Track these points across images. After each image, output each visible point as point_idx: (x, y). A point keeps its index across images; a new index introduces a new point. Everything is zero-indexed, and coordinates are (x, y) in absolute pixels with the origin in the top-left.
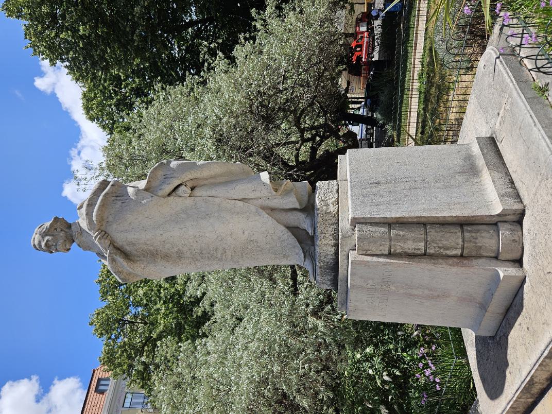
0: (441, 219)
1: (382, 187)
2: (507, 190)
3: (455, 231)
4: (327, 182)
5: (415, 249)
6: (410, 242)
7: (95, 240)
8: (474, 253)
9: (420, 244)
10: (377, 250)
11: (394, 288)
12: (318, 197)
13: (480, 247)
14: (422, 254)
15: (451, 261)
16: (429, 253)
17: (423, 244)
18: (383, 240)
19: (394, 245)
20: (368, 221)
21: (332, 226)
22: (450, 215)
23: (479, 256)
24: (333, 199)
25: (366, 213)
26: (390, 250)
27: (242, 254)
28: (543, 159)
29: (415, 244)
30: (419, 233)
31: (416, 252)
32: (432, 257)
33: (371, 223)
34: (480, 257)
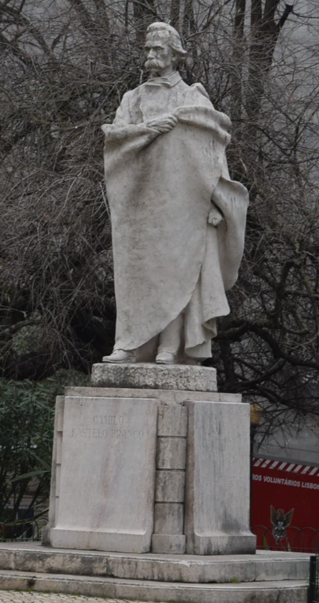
0: (191, 485)
1: (216, 435)
2: (213, 546)
3: (180, 497)
4: (216, 380)
5: (164, 460)
6: (170, 455)
8: (158, 513)
11: (116, 443)
13: (164, 518)
15: (152, 492)
16: (159, 474)
17: (169, 467)
20: (190, 418)
21: (175, 383)
24: (201, 386)
25: (198, 415)
26: (163, 437)
27: (136, 278)
30: (180, 465)
32: (156, 476)
33: (188, 421)
34: (155, 519)
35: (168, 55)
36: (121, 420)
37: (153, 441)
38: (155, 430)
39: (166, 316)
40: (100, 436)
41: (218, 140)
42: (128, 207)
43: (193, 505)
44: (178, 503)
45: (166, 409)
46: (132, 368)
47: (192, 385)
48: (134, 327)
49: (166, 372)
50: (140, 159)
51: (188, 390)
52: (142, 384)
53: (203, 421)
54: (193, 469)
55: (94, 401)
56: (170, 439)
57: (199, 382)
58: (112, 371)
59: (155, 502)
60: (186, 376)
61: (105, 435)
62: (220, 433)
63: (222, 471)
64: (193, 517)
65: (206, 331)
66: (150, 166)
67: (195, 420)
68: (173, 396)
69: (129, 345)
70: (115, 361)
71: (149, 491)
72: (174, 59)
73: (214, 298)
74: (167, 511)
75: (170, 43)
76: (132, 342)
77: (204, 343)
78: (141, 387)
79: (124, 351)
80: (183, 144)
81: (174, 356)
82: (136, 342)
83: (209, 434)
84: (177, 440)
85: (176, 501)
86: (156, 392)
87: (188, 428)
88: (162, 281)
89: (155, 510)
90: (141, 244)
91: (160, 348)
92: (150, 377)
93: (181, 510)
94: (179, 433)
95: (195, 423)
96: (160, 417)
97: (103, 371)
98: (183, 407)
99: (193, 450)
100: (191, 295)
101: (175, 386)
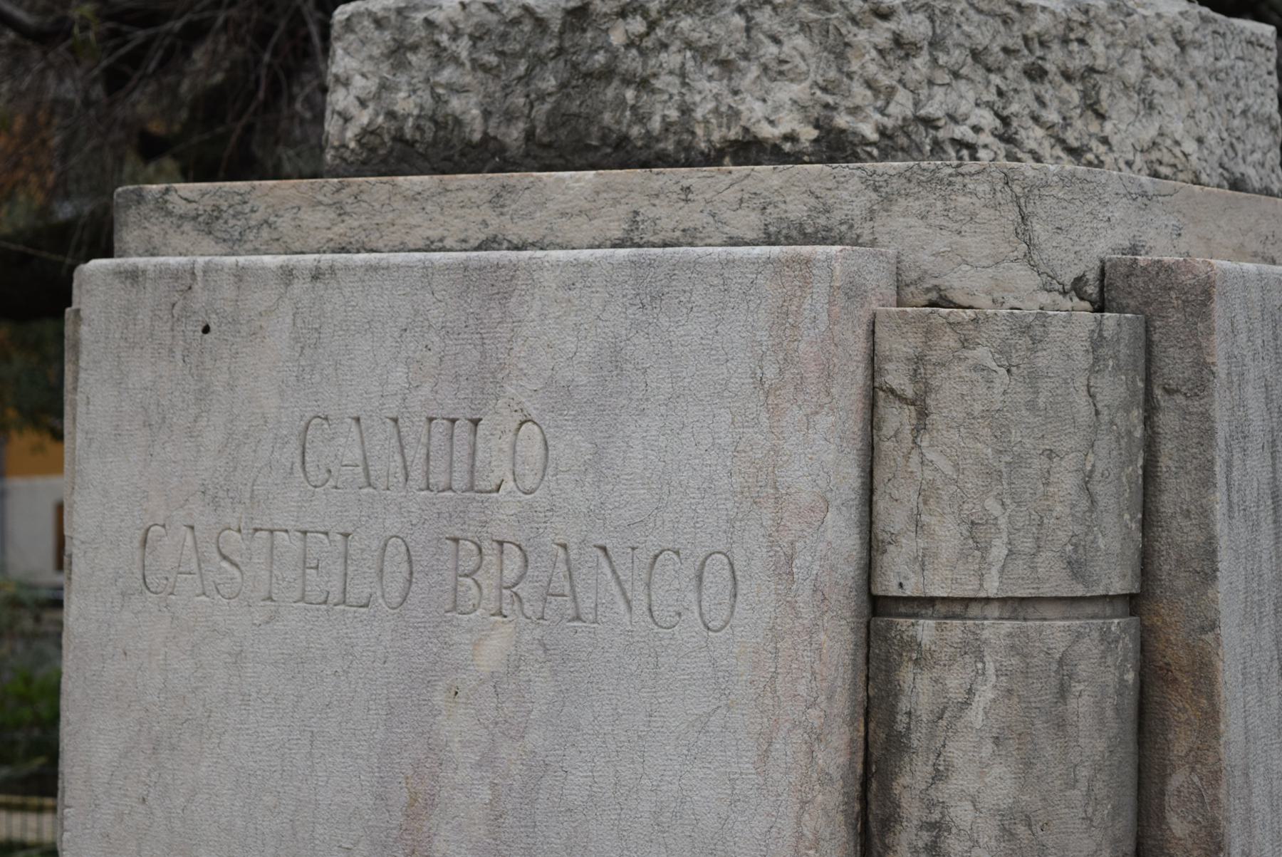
5: (937, 828)
10: (926, 494)
18: (1027, 545)
20: (1168, 421)
21: (986, 119)
24: (1190, 146)
26: (923, 604)
28: (924, 699)
33: (1150, 446)
38: (849, 542)
40: (358, 591)
45: (949, 340)
55: (298, 287)
56: (996, 630)
58: (462, 48)
60: (1077, 63)
61: (395, 589)
67: (1222, 430)
68: (1014, 215)
87: (1148, 518)
92: (778, 71)
94: (1076, 568)
95: (1219, 468)
96: (896, 418)
97: (398, 53)
98: (1110, 318)
99: (1211, 717)
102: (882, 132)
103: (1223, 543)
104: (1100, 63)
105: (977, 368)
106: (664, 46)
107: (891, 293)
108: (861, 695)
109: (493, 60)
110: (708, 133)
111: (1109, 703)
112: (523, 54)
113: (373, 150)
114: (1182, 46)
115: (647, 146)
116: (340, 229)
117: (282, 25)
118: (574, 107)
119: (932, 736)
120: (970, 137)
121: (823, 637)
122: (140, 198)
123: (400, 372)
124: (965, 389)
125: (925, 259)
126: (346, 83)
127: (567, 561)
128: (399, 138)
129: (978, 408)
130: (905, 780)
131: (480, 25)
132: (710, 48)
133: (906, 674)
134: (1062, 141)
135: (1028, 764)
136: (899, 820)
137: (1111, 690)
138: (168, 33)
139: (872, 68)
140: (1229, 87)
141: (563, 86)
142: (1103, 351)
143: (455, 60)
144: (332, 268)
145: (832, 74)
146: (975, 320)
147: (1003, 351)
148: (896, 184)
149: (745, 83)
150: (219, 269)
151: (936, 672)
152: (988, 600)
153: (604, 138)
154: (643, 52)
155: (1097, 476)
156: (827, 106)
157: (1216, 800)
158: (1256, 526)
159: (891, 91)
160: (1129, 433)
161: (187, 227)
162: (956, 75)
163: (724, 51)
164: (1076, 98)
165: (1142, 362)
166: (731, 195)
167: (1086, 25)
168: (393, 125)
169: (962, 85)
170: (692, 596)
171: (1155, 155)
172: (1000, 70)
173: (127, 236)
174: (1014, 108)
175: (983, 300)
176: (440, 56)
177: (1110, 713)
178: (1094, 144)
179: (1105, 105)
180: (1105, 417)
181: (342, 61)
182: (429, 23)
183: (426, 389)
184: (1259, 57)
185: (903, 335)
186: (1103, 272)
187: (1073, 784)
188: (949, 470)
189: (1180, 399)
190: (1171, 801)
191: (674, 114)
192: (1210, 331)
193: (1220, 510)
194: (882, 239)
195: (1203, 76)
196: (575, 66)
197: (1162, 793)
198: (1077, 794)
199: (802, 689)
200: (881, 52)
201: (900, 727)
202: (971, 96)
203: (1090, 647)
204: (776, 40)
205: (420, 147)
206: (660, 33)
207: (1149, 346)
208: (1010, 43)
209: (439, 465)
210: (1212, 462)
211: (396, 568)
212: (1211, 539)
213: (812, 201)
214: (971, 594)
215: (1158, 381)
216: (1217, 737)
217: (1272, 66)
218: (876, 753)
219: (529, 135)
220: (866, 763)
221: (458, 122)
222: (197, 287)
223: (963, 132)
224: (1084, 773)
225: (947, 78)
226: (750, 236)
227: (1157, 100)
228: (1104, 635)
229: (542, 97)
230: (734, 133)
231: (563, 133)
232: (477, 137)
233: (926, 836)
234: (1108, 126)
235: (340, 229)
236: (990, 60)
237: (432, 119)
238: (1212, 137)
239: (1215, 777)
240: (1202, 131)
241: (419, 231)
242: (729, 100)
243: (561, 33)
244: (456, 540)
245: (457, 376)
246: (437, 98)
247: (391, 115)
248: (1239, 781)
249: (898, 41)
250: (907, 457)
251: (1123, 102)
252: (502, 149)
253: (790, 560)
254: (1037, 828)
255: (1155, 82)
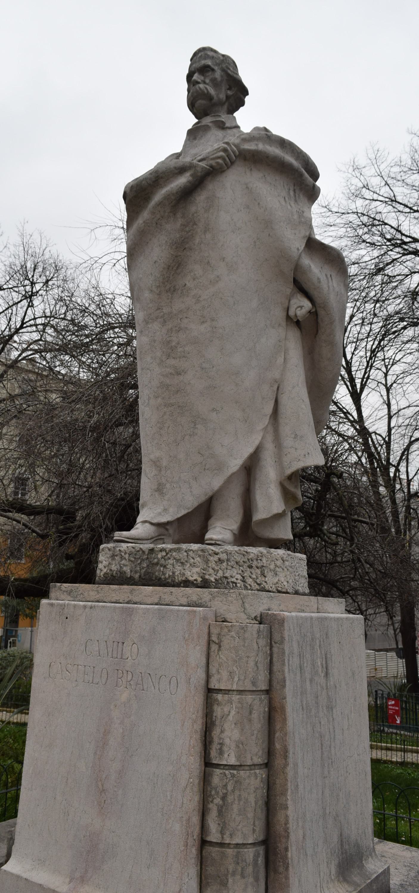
1: (322, 680)
3: (257, 829)
5: (222, 744)
7: (224, 143)
8: (210, 870)
9: (233, 755)
10: (220, 665)
11: (124, 697)
12: (289, 555)
14: (210, 759)
15: (196, 820)
17: (232, 761)
18: (243, 678)
19: (230, 702)
20: (275, 650)
21: (239, 577)
22: (291, 819)
23: (204, 882)
24: (285, 583)
26: (219, 691)
28: (219, 713)
29: (233, 746)
31: (215, 747)
33: (271, 655)
35: (222, 81)
36: (135, 650)
37: (199, 699)
38: (203, 676)
39: (220, 467)
40: (96, 680)
41: (301, 189)
42: (159, 294)
43: (286, 849)
44: (254, 844)
45: (226, 630)
46: (161, 550)
47: (270, 581)
48: (168, 486)
49: (224, 556)
50: (179, 215)
51: (263, 590)
52: (179, 579)
53: (301, 656)
54: (286, 765)
55: (87, 610)
56: (235, 697)
57: (282, 577)
58: (127, 556)
59: (204, 843)
60: (259, 565)
61: (104, 681)
62: (327, 674)
63: (333, 751)
64: (287, 878)
65: (287, 495)
66: (195, 224)
67: (287, 652)
68: (241, 602)
69: (160, 514)
70: (136, 540)
71: (188, 820)
72: (230, 93)
73: (302, 437)
74: (231, 868)
75: (224, 66)
76: (165, 510)
77: (284, 511)
78: (177, 585)
79: (152, 524)
80: (247, 188)
81: (234, 534)
82: (171, 510)
83: (311, 681)
84: (249, 698)
85: (250, 841)
86: (204, 594)
88: (214, 410)
89: (202, 861)
90: (180, 350)
91: (210, 522)
92: (193, 565)
93: (261, 860)
94: (254, 683)
95: (286, 661)
96: (214, 647)
97: (113, 556)
99: (285, 720)
100: (261, 434)
101: (240, 584)
102: (216, 580)
103: (287, 679)
104: (265, 565)
105: (232, 637)
106: (169, 559)
107: (214, 619)
108: (205, 711)
109: (133, 559)
110: (178, 578)
111: (261, 716)
112: (140, 558)
113: (106, 578)
114: (283, 561)
115: (165, 580)
116: (98, 596)
117: (97, 534)
118: (150, 571)
119: (221, 722)
120: (235, 581)
121: (196, 698)
122: (55, 586)
123: (108, 630)
124: (229, 641)
125: (222, 611)
126: (102, 563)
127: (142, 676)
128: (112, 575)
129: (232, 646)
130: (215, 732)
131: (130, 551)
132: (180, 560)
133: (215, 707)
134: (256, 582)
135: (242, 730)
136: (213, 742)
137: (262, 713)
138: (71, 537)
139: (214, 566)
140: (295, 570)
141: (148, 566)
142: (260, 634)
143: (125, 559)
144: (94, 606)
145: (205, 566)
146: (231, 626)
147: (238, 633)
148: (216, 594)
149: (186, 567)
150: (70, 605)
151: (222, 707)
152: (234, 690)
153: (156, 578)
154: (165, 560)
155: (259, 662)
156: (204, 573)
157: (286, 740)
158: (296, 674)
159: (218, 571)
160: (266, 652)
161: (65, 593)
162: (232, 567)
163: (182, 560)
164: (259, 573)
165: (269, 636)
166: (181, 594)
167: (262, 556)
168: (111, 572)
169: (234, 569)
170: (168, 686)
171: (277, 585)
172: (242, 566)
173: (52, 594)
174: (245, 574)
175: (234, 621)
176: (122, 558)
177: (262, 718)
178: (263, 583)
179: (266, 574)
180: (260, 649)
181: (101, 558)
182: (120, 550)
183: (113, 635)
184: (302, 562)
185: (216, 628)
186: (261, 615)
187: (253, 735)
188: (225, 660)
189: (278, 645)
190: (276, 740)
191: (171, 574)
192: (284, 630)
193: (286, 670)
194: (213, 606)
195: (289, 568)
196: (150, 562)
197: (274, 738)
198: (254, 737)
199: (191, 710)
200: (216, 562)
201: (214, 720)
202: (236, 572)
203: (257, 702)
204: (193, 559)
205: (117, 578)
206: (169, 555)
207: (271, 632)
208: (245, 560)
209: (115, 652)
210: (284, 660)
211: (104, 675)
212: (284, 678)
213: (198, 597)
214: (229, 689)
215: (273, 640)
216: (286, 725)
217: (305, 564)
218: (208, 726)
219: (140, 576)
220: (206, 728)
221: (125, 573)
222: (66, 608)
223: (234, 580)
224: (255, 732)
225: (230, 568)
226: (185, 604)
227: (278, 573)
228: (260, 699)
229: (143, 568)
230: (184, 579)
231: (147, 576)
232: (129, 576)
233: (219, 746)
234: (267, 579)
235: (98, 596)
236: (240, 564)
237: (120, 571)
238: (290, 581)
239: (286, 734)
240: (288, 580)
241: (114, 598)
242: (183, 571)
243: (148, 554)
244: (118, 670)
245: (120, 632)
246: (121, 567)
247: (111, 570)
248: (292, 735)
249: (219, 559)
250: (216, 656)
251: (270, 573)
252: (134, 579)
253: (190, 679)
254: (244, 745)
255: (277, 569)
